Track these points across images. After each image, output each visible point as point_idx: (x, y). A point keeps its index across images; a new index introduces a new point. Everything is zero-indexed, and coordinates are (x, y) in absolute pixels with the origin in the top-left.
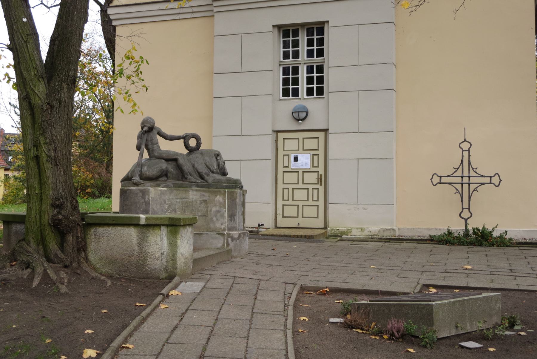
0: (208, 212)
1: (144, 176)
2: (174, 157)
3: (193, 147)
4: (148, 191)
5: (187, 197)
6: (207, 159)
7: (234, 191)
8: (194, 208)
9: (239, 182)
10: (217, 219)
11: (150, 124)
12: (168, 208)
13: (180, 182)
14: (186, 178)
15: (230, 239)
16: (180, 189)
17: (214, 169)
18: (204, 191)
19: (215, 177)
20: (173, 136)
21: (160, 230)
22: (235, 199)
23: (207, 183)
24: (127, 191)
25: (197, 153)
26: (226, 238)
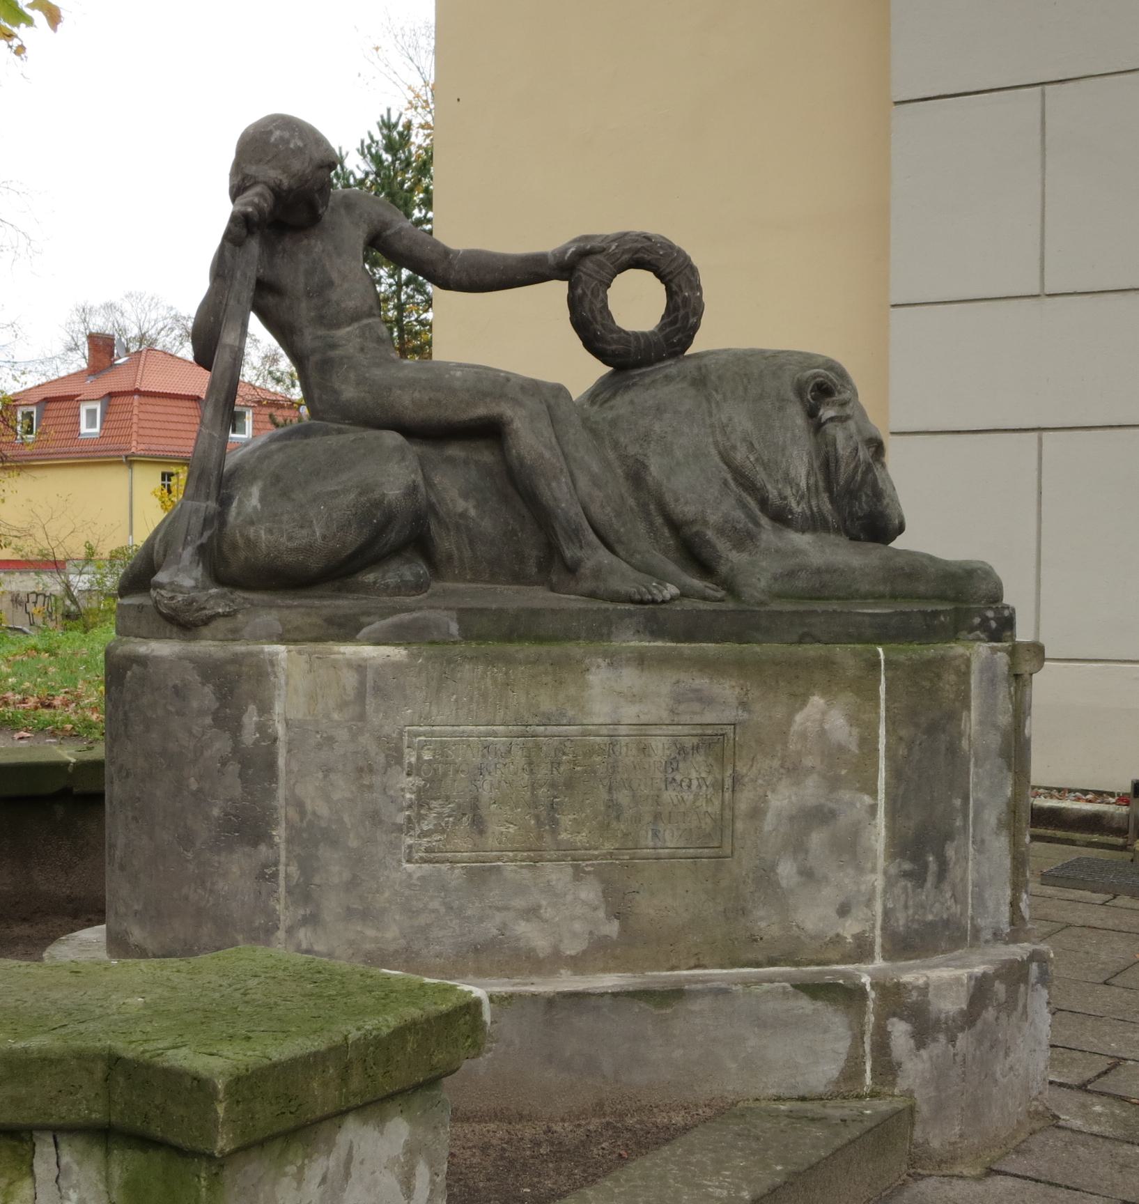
0: (739, 825)
1: (242, 555)
2: (481, 411)
3: (636, 335)
4: (261, 672)
5: (571, 713)
6: (738, 417)
7: (943, 660)
8: (623, 797)
9: (984, 588)
10: (807, 874)
11: (285, 169)
12: (423, 800)
13: (538, 597)
14: (572, 569)
15: (899, 1030)
16: (511, 648)
17: (788, 492)
18: (706, 665)
19: (796, 552)
20: (494, 255)
21: (31, 1173)
22: (953, 717)
23: (730, 605)
24: (126, 669)
25: (668, 379)
26: (871, 1018)
